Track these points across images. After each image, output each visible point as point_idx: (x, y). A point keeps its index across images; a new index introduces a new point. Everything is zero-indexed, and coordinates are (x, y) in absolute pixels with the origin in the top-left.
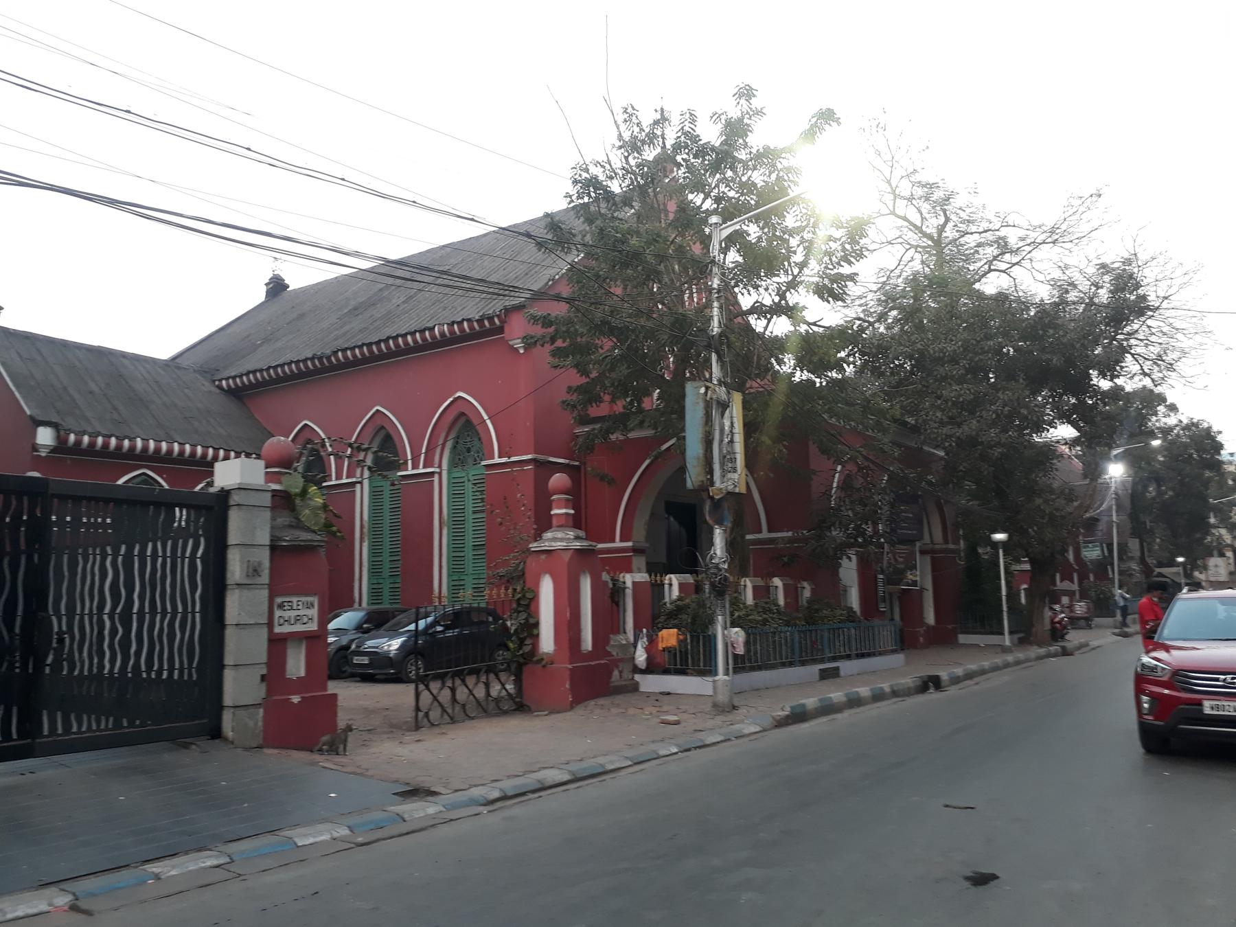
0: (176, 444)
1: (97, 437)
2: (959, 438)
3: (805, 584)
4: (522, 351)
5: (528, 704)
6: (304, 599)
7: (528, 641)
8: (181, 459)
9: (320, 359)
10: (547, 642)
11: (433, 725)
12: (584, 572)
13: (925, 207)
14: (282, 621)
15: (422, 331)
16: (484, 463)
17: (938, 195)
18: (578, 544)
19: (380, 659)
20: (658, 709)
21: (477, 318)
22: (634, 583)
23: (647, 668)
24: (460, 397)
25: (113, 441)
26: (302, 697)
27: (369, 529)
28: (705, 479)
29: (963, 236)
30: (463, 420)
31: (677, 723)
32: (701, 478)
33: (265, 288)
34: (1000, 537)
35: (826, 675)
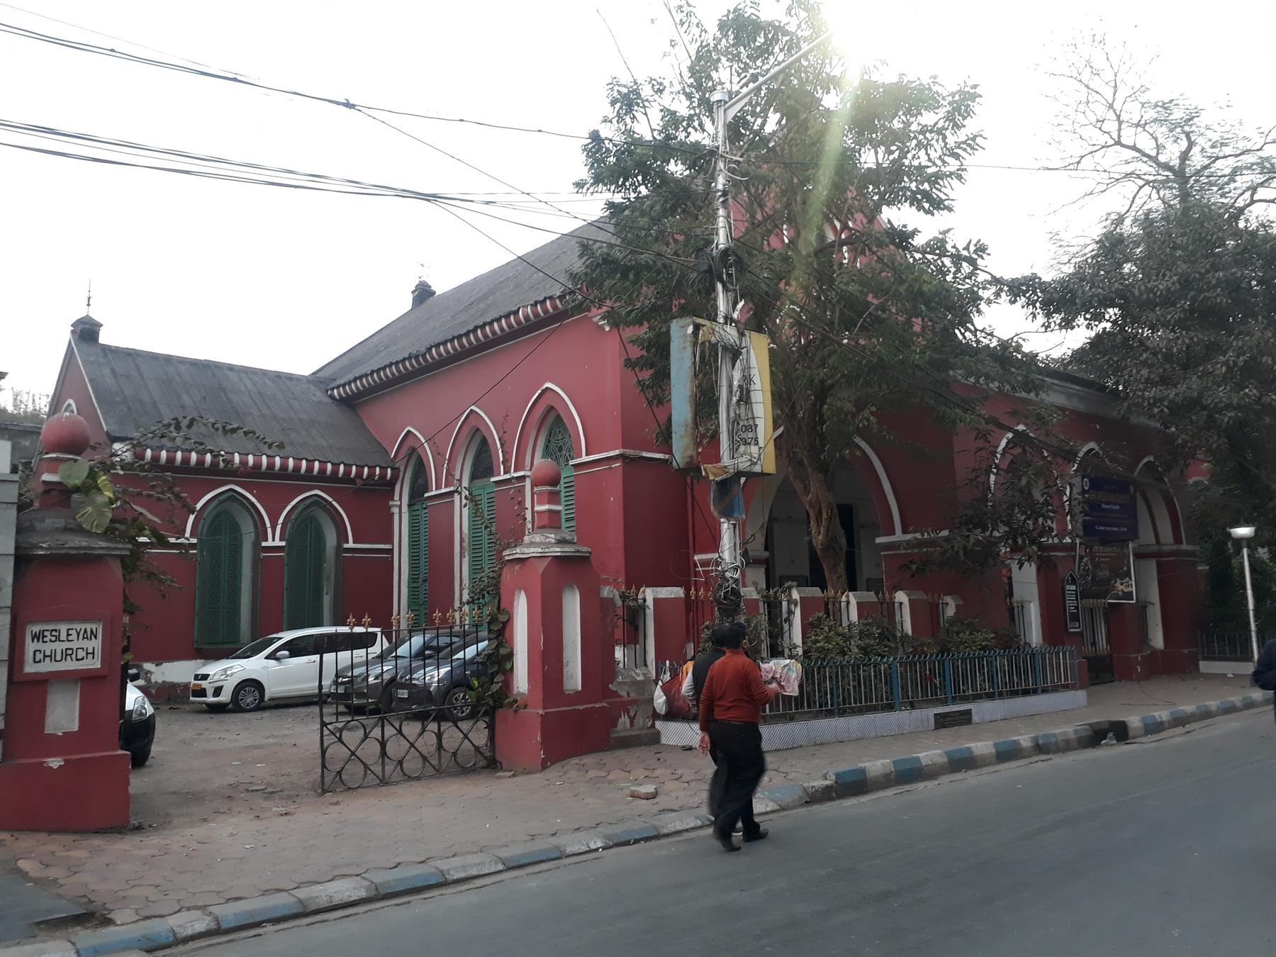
0: (264, 457)
1: (176, 452)
2: (1171, 402)
3: (948, 599)
4: (607, 329)
5: (500, 760)
6: (81, 626)
7: (499, 678)
8: (270, 472)
9: (416, 357)
10: (521, 681)
11: (410, 778)
12: (571, 586)
13: (1160, 131)
14: (39, 656)
15: (507, 316)
16: (571, 462)
17: (1178, 115)
18: (559, 550)
19: (421, 694)
20: (647, 773)
21: (558, 294)
22: (656, 600)
23: (666, 714)
24: (547, 388)
25: (194, 456)
26: (65, 760)
27: (469, 542)
28: (694, 453)
29: (1214, 162)
30: (552, 416)
31: (653, 796)
32: (689, 453)
33: (411, 297)
34: (1244, 531)
35: (943, 722)
